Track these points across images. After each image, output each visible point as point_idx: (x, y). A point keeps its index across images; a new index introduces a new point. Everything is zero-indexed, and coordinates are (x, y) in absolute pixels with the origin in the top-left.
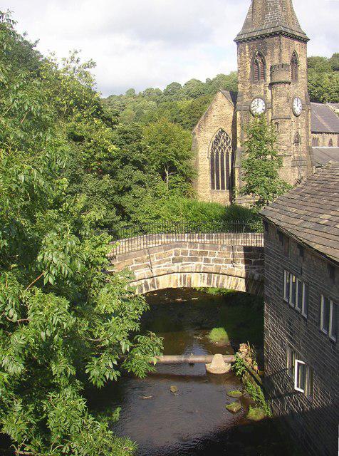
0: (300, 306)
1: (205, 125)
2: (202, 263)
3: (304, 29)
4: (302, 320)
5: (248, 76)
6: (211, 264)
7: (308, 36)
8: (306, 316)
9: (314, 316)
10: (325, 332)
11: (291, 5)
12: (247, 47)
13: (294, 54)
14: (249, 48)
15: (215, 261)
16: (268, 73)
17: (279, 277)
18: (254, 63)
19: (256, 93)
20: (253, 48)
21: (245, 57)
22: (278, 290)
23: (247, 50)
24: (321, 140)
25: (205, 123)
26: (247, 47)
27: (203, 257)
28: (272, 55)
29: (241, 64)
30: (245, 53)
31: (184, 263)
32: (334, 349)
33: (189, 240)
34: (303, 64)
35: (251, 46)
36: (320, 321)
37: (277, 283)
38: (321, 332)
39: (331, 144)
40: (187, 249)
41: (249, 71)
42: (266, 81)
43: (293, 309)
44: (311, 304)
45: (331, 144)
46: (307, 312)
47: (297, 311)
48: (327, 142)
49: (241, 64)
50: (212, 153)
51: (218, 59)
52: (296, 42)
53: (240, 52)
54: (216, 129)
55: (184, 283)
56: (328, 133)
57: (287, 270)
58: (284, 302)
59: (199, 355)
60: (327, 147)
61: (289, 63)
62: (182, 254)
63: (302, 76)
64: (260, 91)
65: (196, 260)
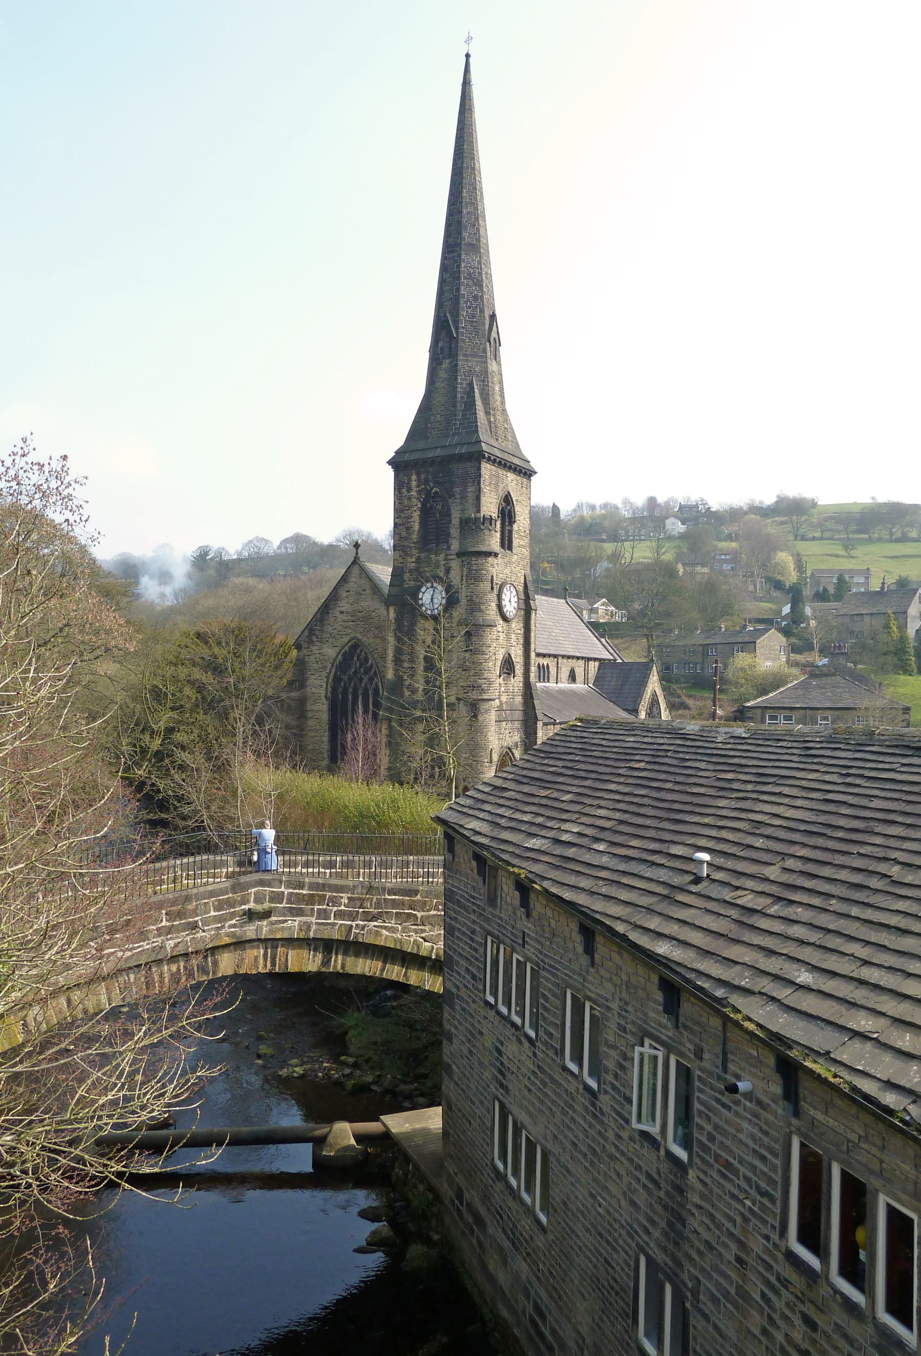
0: (522, 1014)
1: (322, 631)
2: (313, 920)
3: (527, 452)
4: (526, 1044)
5: (415, 536)
6: (332, 920)
7: (534, 465)
8: (532, 1034)
9: (550, 1035)
10: (574, 1068)
11: (503, 403)
12: (414, 477)
13: (507, 499)
14: (419, 480)
15: (340, 915)
16: (454, 531)
17: (476, 950)
18: (426, 512)
19: (428, 571)
20: (426, 482)
21: (409, 499)
22: (474, 977)
23: (414, 483)
24: (553, 670)
25: (322, 626)
26: (414, 477)
27: (316, 907)
28: (464, 497)
29: (402, 511)
30: (409, 489)
31: (273, 919)
32: (594, 1105)
33: (286, 870)
34: (522, 522)
35: (423, 476)
36: (564, 1044)
37: (471, 963)
38: (565, 1069)
39: (572, 677)
40: (31, 675)
41: (416, 526)
42: (449, 548)
43: (506, 1019)
44: (546, 1009)
45: (572, 677)
46: (535, 1026)
47: (513, 1024)
48: (564, 674)
49: (402, 511)
50: (334, 690)
51: (362, 508)
52: (511, 476)
53: (400, 486)
54: (346, 639)
55: (273, 964)
56: (569, 657)
57: (492, 935)
58: (487, 1003)
59: (651, 1343)
60: (564, 685)
61: (495, 515)
62: (272, 900)
63: (520, 541)
64: (437, 566)
65: (300, 913)
